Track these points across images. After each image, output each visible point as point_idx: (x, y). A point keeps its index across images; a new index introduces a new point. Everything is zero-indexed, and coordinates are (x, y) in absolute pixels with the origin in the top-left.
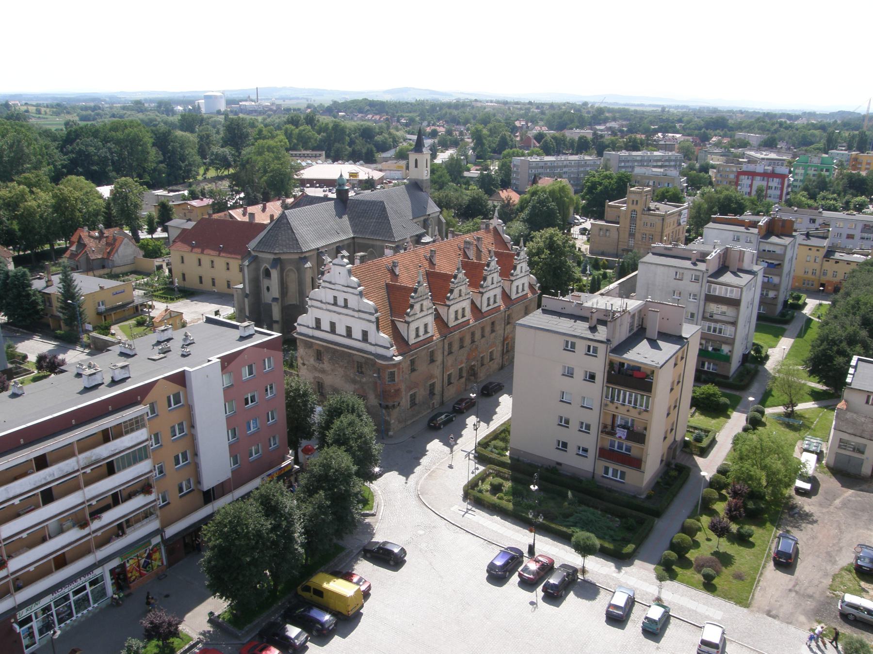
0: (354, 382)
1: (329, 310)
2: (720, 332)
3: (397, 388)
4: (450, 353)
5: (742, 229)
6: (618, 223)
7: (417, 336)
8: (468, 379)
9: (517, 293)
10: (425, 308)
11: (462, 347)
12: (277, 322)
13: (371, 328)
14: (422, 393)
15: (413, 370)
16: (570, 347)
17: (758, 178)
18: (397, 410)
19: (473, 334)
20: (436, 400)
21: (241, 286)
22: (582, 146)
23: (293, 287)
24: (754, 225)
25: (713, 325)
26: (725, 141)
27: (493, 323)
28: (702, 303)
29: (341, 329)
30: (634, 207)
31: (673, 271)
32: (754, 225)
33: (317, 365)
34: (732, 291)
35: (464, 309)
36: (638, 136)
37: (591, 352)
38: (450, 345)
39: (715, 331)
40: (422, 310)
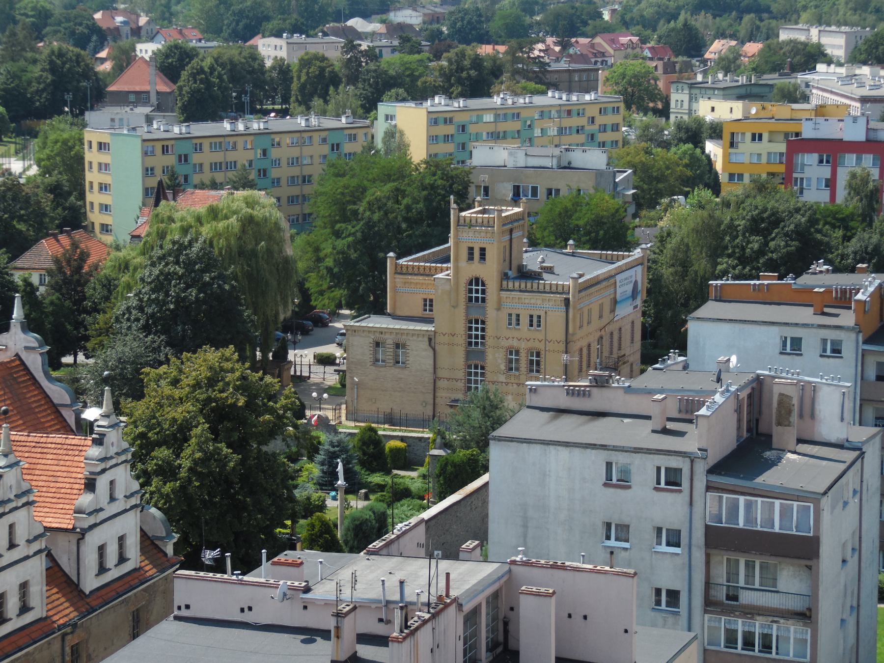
2: (766, 646)
5: (805, 314)
6: (429, 321)
9: (102, 569)
17: (850, 159)
22: (315, 85)
24: (844, 299)
25: (740, 626)
26: (753, 48)
28: (699, 556)
30: (476, 269)
31: (598, 459)
32: (844, 299)
34: (785, 513)
35: (121, 539)
36: (485, 50)
39: (749, 643)
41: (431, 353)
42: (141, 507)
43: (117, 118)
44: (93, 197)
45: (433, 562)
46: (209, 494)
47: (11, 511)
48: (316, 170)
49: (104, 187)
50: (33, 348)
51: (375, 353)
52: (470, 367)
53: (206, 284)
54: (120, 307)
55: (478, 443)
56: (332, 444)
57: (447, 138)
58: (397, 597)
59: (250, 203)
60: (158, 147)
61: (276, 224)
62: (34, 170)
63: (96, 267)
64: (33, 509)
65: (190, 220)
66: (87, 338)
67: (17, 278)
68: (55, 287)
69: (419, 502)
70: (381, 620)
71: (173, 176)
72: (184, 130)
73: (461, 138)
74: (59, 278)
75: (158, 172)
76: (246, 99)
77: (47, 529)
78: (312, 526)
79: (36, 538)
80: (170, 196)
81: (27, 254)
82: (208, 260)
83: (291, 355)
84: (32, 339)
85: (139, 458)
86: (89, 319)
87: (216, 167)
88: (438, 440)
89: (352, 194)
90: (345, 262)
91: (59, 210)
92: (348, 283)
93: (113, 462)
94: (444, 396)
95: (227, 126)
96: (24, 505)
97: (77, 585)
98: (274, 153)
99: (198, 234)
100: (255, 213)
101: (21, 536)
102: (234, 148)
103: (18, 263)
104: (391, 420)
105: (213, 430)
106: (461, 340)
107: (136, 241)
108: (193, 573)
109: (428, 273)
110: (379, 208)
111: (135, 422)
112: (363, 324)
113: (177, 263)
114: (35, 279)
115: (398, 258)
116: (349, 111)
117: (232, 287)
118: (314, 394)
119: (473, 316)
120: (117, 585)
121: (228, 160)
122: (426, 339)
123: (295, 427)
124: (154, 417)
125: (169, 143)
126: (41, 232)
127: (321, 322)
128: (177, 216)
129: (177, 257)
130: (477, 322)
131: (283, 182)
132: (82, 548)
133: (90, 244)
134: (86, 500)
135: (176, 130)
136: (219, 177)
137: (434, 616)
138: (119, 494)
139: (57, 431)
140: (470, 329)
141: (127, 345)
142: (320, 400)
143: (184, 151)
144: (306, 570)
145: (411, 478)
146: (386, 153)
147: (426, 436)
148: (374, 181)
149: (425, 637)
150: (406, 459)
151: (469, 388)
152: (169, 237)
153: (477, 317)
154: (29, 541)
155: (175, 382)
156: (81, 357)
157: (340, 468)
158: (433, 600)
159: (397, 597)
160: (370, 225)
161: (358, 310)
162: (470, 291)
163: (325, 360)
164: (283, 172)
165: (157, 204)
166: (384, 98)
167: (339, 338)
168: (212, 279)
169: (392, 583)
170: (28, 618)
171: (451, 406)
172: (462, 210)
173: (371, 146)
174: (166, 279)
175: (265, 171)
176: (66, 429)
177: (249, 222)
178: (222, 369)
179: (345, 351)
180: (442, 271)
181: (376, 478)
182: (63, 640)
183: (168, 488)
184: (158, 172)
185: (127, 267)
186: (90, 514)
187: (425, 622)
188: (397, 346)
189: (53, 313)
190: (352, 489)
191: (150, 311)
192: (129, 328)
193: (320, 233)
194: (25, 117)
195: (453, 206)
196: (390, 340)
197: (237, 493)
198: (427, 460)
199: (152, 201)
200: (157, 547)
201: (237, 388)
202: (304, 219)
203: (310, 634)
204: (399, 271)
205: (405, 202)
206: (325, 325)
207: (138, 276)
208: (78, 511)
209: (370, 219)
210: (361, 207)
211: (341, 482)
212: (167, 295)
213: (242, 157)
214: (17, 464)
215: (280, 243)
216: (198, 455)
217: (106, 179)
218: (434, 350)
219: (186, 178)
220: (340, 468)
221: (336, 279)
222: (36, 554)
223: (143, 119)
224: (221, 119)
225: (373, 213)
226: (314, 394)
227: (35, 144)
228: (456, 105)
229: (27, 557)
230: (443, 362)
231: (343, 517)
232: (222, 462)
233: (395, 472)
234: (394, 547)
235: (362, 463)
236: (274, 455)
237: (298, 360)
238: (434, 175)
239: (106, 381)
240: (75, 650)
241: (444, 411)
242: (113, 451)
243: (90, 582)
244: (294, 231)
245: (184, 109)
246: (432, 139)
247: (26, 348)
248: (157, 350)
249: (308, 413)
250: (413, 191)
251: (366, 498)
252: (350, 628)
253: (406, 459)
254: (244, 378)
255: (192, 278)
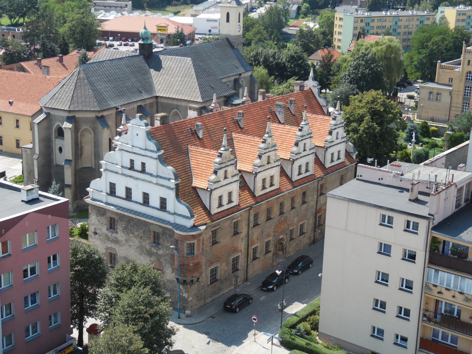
0: (150, 254)
1: (157, 184)
3: (196, 261)
4: (256, 225)
6: (451, 86)
7: (220, 205)
8: (275, 254)
9: (300, 174)
10: (229, 175)
11: (269, 219)
12: (69, 186)
13: (171, 196)
14: (223, 268)
15: (215, 243)
16: (387, 222)
18: (196, 286)
19: (282, 205)
20: (241, 274)
21: (31, 146)
23: (88, 149)
27: (304, 194)
29: (137, 196)
33: (110, 234)
37: (410, 228)
38: (256, 216)
40: (226, 178)
41: (450, 97)
42: (346, 142)
43: (346, 9)
44: (336, 36)
45: (448, 170)
46: (369, 140)
47: (305, 139)
48: (414, 30)
49: (340, 33)
50: (315, 86)
51: (430, 96)
52: (464, 103)
53: (372, 68)
54: (342, 74)
55: (464, 130)
56: (411, 126)
57: (463, 20)
58: (434, 180)
59: (390, 41)
60: (360, 20)
61: (398, 48)
62: (317, 26)
63: (335, 60)
64: (312, 139)
65: (369, 45)
66: (330, 84)
67: (310, 62)
68: (322, 66)
69: (440, 149)
70: (427, 188)
71: (364, 30)
72: (369, 14)
73: (468, 21)
74: (323, 63)
75: (359, 28)
76: (391, 4)
77: (281, 158)
78: (402, 154)
79: (312, 149)
80: (362, 37)
81: (313, 55)
82: (373, 60)
83: (399, 95)
84: (315, 83)
85: (347, 125)
86: (332, 78)
87: (378, 27)
88: (450, 128)
89: (427, 39)
90: (421, 63)
91: (324, 40)
92: (422, 70)
93: (338, 126)
94: (453, 113)
95: (384, 13)
96: (309, 137)
97: (291, 179)
98: (399, 23)
99: (371, 50)
100: (391, 44)
101: (308, 148)
102: (386, 21)
103: (310, 57)
104: (433, 120)
105: (372, 118)
106: (462, 93)
107: (350, 52)
108: (364, 165)
109: (452, 69)
110: (436, 45)
111: (346, 114)
112: (426, 85)
113: (363, 60)
114: (315, 64)
115: (441, 63)
116: (428, 10)
117: (381, 69)
118: (406, 109)
119: (467, 85)
120: (336, 166)
121: (383, 25)
122: (449, 92)
123: (400, 119)
124: (352, 112)
125: (363, 19)
126: (318, 47)
127: (410, 84)
128: (364, 44)
129: (363, 58)
130: (468, 87)
131: (402, 34)
132: (326, 154)
133: (334, 52)
134: (329, 138)
135: (366, 14)
136: (379, 31)
137: (447, 188)
138: (340, 137)
139: (321, 114)
140: (466, 90)
141: (344, 87)
142: (408, 111)
143: (367, 22)
144: (402, 168)
145: (439, 141)
146: (440, 25)
147: (445, 126)
148: (435, 34)
149: (443, 195)
150: (437, 134)
151: (463, 111)
152: (361, 51)
153: (468, 85)
154: (310, 149)
155: (360, 101)
156: (328, 91)
157: (414, 135)
158: (447, 183)
159: (434, 180)
160: (432, 50)
161: (424, 80)
162: (467, 76)
163: (411, 97)
164: (402, 30)
165: (358, 40)
166: (441, 5)
167: (416, 90)
168: (374, 66)
169: (433, 175)
170: (308, 174)
171: (456, 117)
172: (467, 47)
173: (435, 22)
174: (359, 66)
175: (395, 30)
176: (324, 114)
177: (389, 47)
178: (377, 98)
179: (418, 95)
180: (457, 68)
181: (426, 140)
182: (318, 182)
183: (355, 136)
184: (359, 28)
185: (345, 61)
186: (330, 142)
187: (443, 190)
188: (438, 94)
189: (320, 75)
190: (417, 143)
191: (352, 76)
192: (345, 82)
193: (413, 52)
194: (316, 8)
195: (464, 45)
196: (435, 92)
197: (378, 140)
198: (445, 135)
199: (356, 38)
200: (350, 155)
201: (381, 105)
202: (408, 47)
203: (402, 190)
204: (441, 67)
205: (446, 43)
206: (412, 85)
207: (349, 64)
208: (326, 141)
209: (432, 48)
210: (429, 44)
211: (414, 140)
212: (358, 71)
213: (388, 24)
214: (308, 124)
215: (399, 55)
216: (366, 126)
217: (341, 30)
218: (451, 96)
219: (368, 31)
220: (414, 135)
221: (418, 69)
222: (312, 154)
223: (355, 10)
224: (382, 11)
225: (433, 46)
226: (406, 109)
227: (318, 17)
228: (468, 8)
229: (309, 154)
230: (454, 100)
231: (413, 152)
232: (374, 129)
233: (433, 138)
234: (434, 163)
235: (421, 134)
236: (392, 129)
237: (401, 96)
238: (457, 33)
239: (337, 99)
240: (322, 186)
241: (452, 118)
242: (338, 122)
243: (328, 165)
244: (404, 51)
245: (369, 7)
246: (457, 20)
247: (313, 86)
248: (353, 90)
249: (403, 115)
250: (449, 39)
251: (422, 146)
252: (417, 189)
253: (437, 134)
254: (384, 101)
255: (367, 66)
